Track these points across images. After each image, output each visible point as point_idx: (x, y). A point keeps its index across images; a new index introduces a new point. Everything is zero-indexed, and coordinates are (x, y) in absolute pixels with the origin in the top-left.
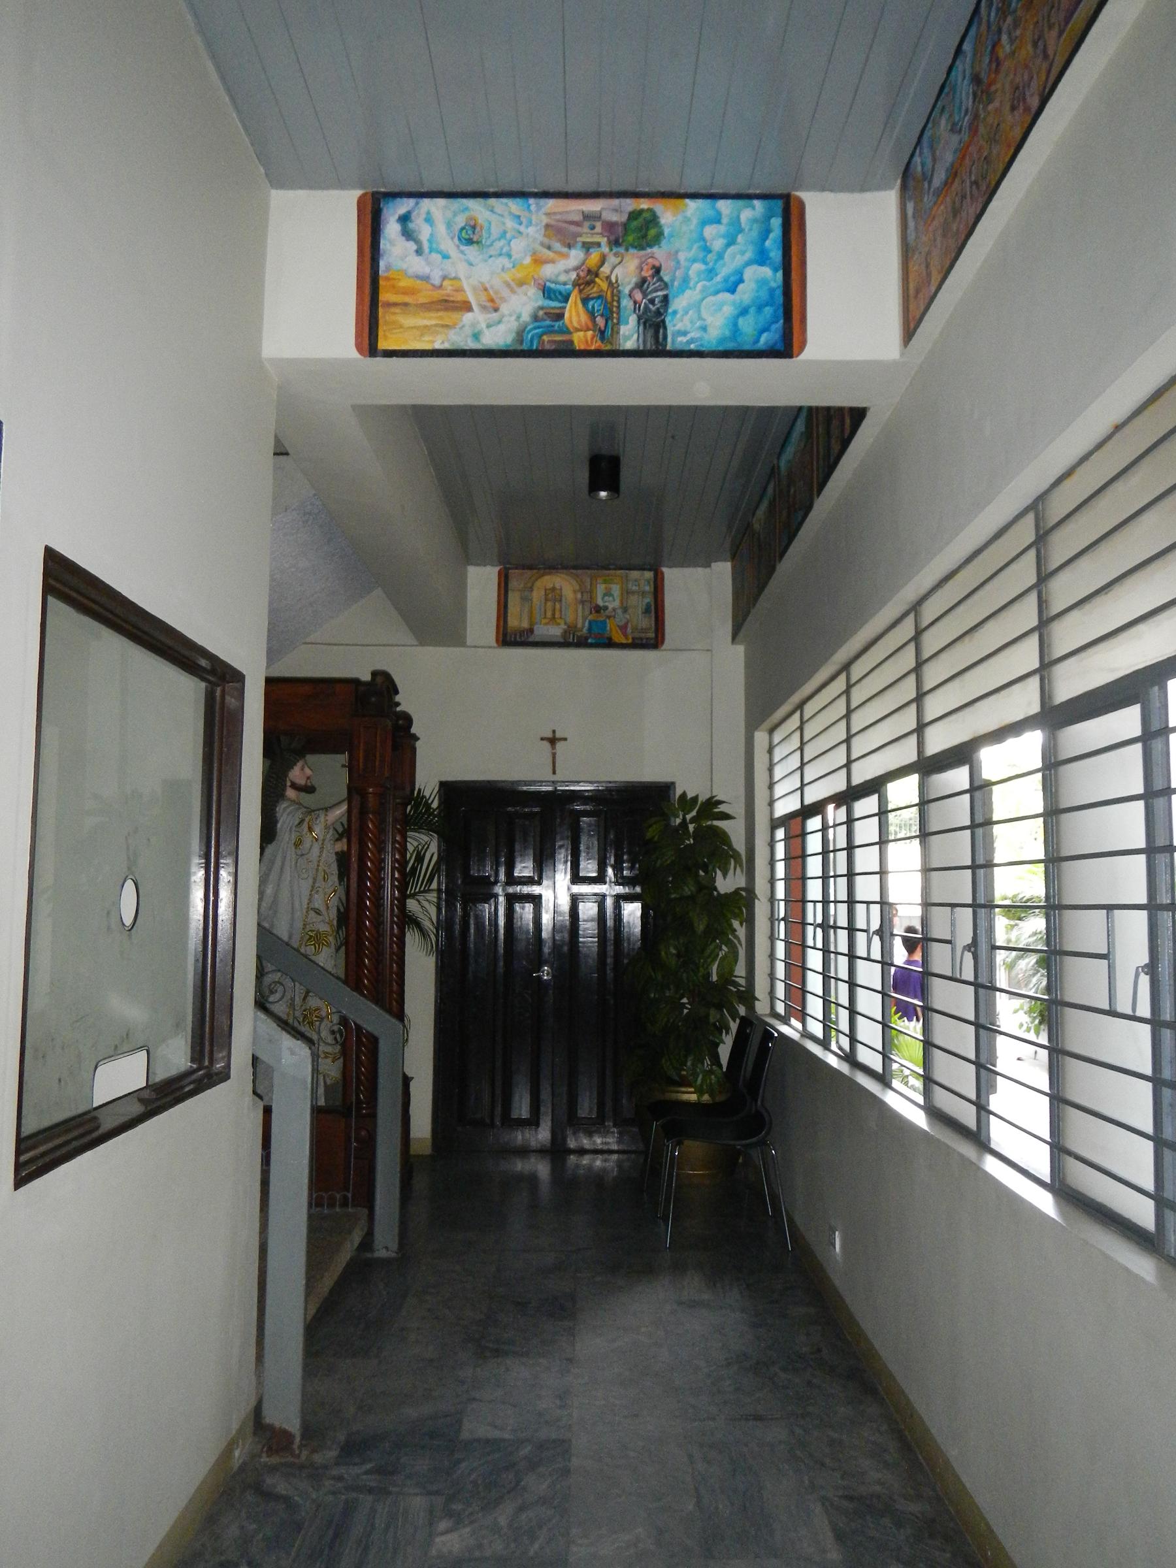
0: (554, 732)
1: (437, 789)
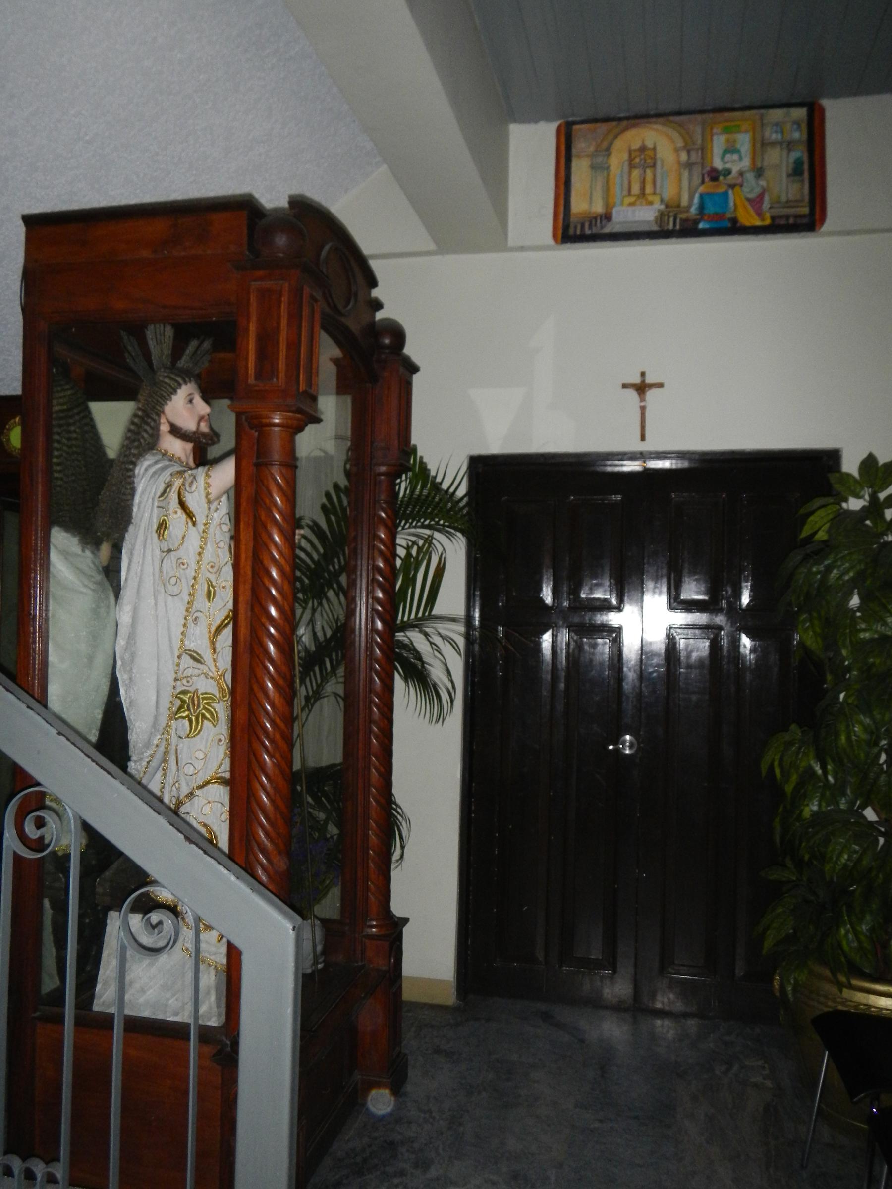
0: (643, 374)
1: (464, 468)
